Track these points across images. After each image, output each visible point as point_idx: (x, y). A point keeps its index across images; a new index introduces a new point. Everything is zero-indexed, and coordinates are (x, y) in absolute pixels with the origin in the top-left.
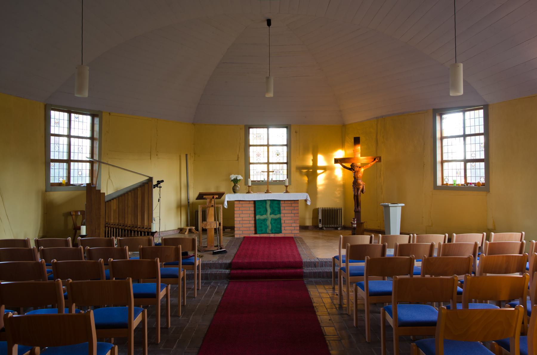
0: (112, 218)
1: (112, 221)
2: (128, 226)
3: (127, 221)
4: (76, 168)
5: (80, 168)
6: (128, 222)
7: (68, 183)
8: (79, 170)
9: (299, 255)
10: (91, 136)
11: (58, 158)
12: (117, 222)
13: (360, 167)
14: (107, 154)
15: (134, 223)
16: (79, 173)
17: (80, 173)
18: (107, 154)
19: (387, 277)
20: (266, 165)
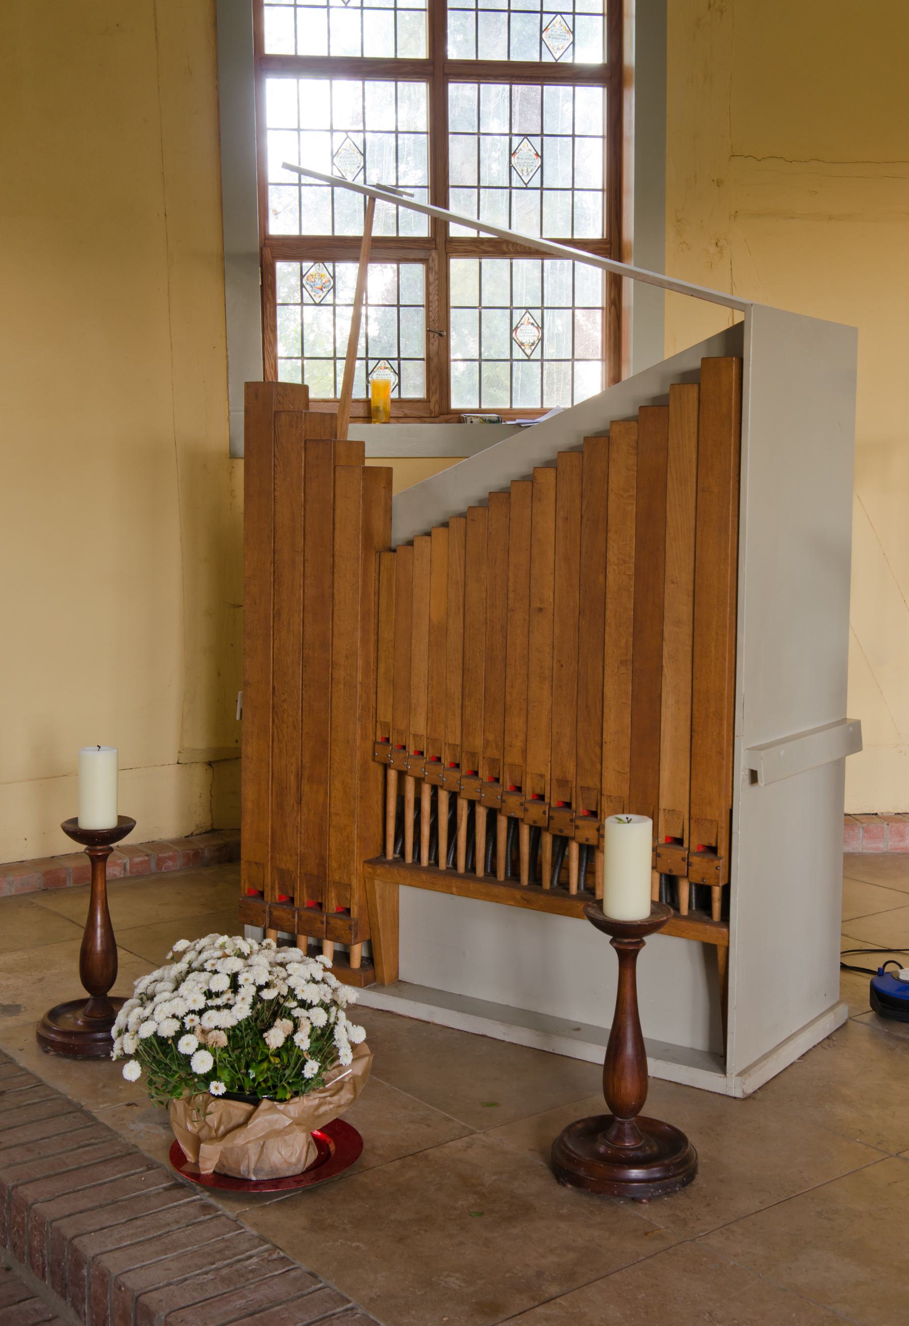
0: (421, 697)
1: (420, 725)
2: (529, 787)
3: (518, 743)
4: (496, 294)
5: (526, 296)
6: (524, 752)
7: (427, 401)
8: (517, 314)
9: (21, 865)
10: (606, 62)
11: (325, 231)
12: (455, 738)
13: (463, 164)
14: (719, 183)
15: (571, 768)
16: (520, 336)
17: (527, 334)
18: (719, 183)
19: (213, 1179)
20: (297, 187)
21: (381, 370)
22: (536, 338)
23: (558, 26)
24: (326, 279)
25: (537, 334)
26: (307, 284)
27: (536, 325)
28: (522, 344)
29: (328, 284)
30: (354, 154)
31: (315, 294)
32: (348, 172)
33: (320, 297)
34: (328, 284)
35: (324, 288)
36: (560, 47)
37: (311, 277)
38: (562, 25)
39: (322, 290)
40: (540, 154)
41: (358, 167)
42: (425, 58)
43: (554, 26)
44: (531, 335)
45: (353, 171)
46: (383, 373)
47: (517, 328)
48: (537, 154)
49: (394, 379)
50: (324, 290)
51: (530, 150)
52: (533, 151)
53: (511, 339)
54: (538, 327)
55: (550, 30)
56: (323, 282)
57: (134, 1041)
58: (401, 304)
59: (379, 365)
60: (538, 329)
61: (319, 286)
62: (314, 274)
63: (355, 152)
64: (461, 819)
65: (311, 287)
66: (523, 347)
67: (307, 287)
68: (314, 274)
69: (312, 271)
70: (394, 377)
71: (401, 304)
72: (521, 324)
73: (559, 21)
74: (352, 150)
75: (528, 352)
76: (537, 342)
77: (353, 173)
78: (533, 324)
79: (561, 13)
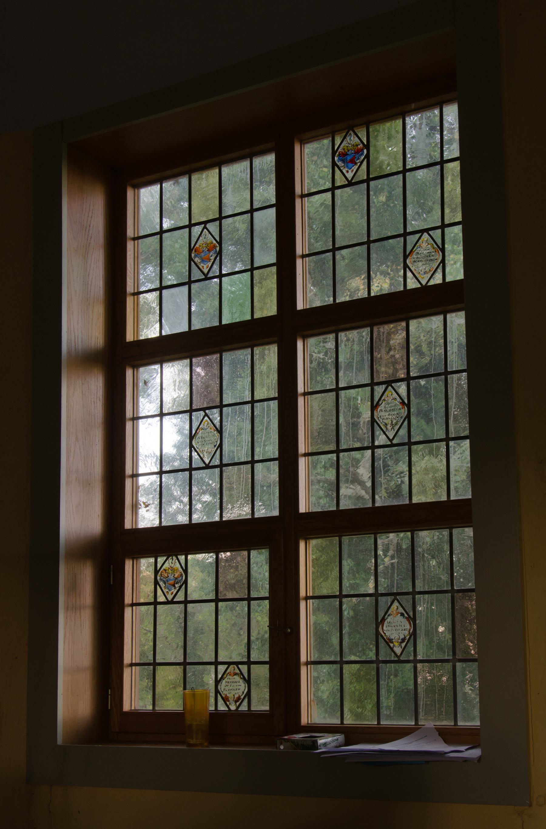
21: (230, 677)
22: (407, 632)
23: (424, 245)
24: (178, 574)
25: (408, 627)
26: (161, 579)
27: (406, 615)
28: (391, 641)
29: (180, 578)
30: (211, 432)
31: (167, 590)
32: (205, 453)
33: (172, 593)
34: (180, 578)
35: (177, 584)
36: (427, 269)
37: (164, 572)
38: (428, 244)
39: (174, 585)
40: (406, 401)
41: (215, 446)
42: (276, 348)
43: (420, 246)
44: (400, 628)
45: (210, 450)
46: (232, 680)
47: (383, 620)
48: (403, 403)
49: (242, 687)
50: (176, 586)
51: (395, 399)
52: (398, 399)
53: (378, 634)
54: (409, 619)
55: (414, 253)
56: (176, 576)
57: (177, 428)
58: (252, 602)
59: (228, 671)
60: (408, 620)
61: (172, 582)
62: (167, 569)
63: (212, 430)
64: (451, 417)
65: (165, 583)
66: (392, 645)
67: (161, 583)
68: (167, 569)
69: (166, 566)
70: (243, 685)
71: (252, 602)
72: (389, 615)
73: (426, 239)
74: (209, 429)
75: (398, 650)
76: (408, 637)
77: (210, 453)
78: (402, 614)
79: (427, 230)
